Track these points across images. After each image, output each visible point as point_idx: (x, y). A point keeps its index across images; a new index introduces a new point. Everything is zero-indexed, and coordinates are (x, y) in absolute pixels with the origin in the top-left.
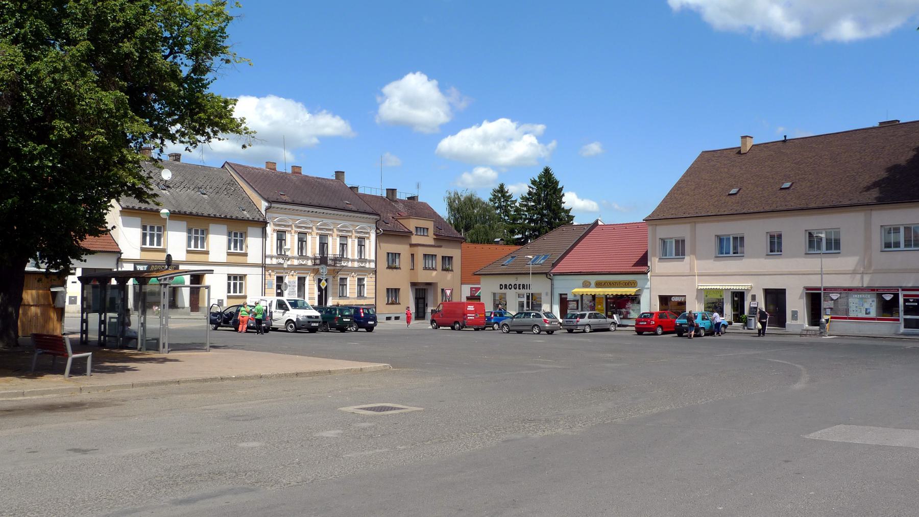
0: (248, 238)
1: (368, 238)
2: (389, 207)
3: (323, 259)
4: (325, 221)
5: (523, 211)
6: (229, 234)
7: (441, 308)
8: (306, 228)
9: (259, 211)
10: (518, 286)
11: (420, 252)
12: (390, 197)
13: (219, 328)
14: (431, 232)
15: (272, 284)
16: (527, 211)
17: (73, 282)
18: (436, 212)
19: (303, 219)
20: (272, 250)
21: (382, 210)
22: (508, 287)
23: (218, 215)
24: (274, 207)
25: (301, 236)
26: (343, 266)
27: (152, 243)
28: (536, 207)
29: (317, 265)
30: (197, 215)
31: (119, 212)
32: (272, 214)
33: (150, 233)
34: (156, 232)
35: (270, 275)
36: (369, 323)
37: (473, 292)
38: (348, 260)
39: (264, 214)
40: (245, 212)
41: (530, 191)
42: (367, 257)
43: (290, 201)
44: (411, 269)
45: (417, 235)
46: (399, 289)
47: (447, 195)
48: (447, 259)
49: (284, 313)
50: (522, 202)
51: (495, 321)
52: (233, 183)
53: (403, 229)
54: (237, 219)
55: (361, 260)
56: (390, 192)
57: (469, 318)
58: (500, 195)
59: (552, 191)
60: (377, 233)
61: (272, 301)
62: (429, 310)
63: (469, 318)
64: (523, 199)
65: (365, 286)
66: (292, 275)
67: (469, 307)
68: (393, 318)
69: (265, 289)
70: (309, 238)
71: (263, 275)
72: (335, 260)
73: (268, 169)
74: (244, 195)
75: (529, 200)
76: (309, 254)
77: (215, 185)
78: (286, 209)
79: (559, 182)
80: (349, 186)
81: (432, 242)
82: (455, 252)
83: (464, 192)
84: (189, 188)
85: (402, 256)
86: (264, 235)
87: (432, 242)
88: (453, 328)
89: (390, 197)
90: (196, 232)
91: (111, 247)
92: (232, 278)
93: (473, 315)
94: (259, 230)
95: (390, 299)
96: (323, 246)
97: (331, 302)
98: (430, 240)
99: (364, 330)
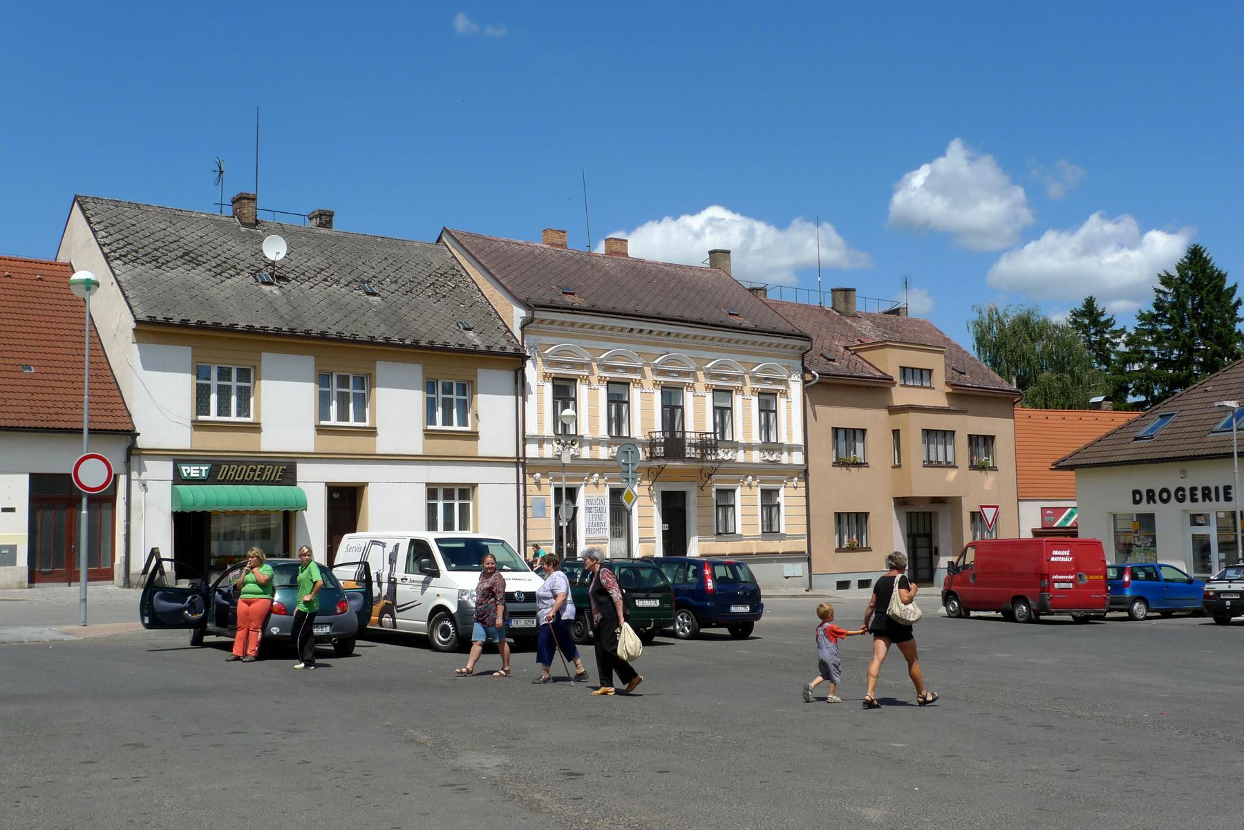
0: (479, 396)
1: (785, 394)
2: (839, 327)
3: (673, 445)
4: (674, 353)
5: (1147, 344)
6: (430, 387)
7: (971, 556)
8: (627, 369)
9: (509, 331)
10: (1188, 493)
11: (914, 425)
12: (842, 307)
13: (207, 639)
14: (939, 378)
15: (544, 507)
16: (1154, 344)
17: (12, 510)
18: (949, 339)
19: (617, 348)
20: (541, 424)
21: (822, 333)
22: (1157, 497)
23: (395, 339)
24: (542, 321)
25: (616, 389)
26: (722, 461)
27: (224, 409)
28: (1176, 333)
29: (657, 458)
30: (340, 339)
31: (132, 331)
32: (538, 337)
33: (219, 386)
34: (234, 383)
35: (538, 484)
36: (734, 609)
37: (1047, 519)
38: (735, 446)
39: (519, 338)
40: (471, 334)
41: (1159, 299)
42: (783, 439)
43: (584, 306)
44: (894, 467)
45: (905, 385)
46: (866, 514)
47: (976, 317)
48: (980, 443)
49: (426, 584)
50: (1141, 325)
51: (1137, 594)
52: (455, 272)
53: (869, 373)
54: (446, 348)
55: (769, 446)
56: (840, 296)
57: (1057, 585)
58: (1087, 321)
59: (1212, 297)
60: (805, 382)
61: (397, 547)
62: (943, 562)
63: (1057, 585)
64: (1144, 319)
65: (782, 508)
66: (596, 484)
67: (1055, 553)
68: (854, 584)
69: (525, 518)
70: (635, 394)
71: (521, 486)
72: (706, 446)
73: (545, 246)
74: (478, 297)
75: (1157, 321)
76: (638, 433)
77: (408, 276)
78: (573, 324)
79: (1225, 275)
80: (748, 286)
81: (943, 402)
82: (1000, 427)
83: (1011, 309)
84: (337, 282)
85: (868, 434)
86: (520, 388)
87: (943, 402)
88: (1009, 617)
89: (842, 307)
90: (343, 381)
91: (112, 420)
92: (440, 494)
93: (1072, 577)
94: (507, 377)
95: (846, 538)
96: (672, 410)
97: (695, 549)
98: (937, 396)
99: (724, 631)
